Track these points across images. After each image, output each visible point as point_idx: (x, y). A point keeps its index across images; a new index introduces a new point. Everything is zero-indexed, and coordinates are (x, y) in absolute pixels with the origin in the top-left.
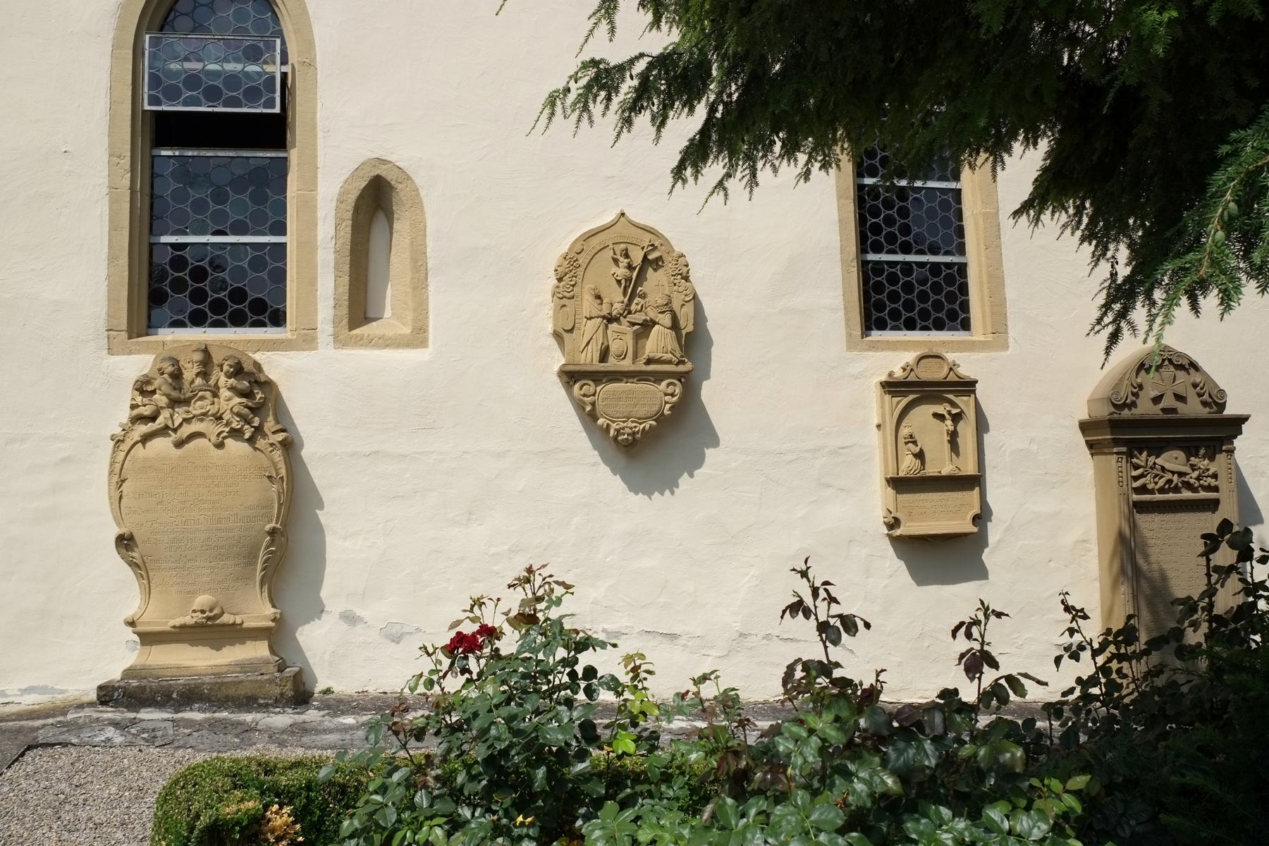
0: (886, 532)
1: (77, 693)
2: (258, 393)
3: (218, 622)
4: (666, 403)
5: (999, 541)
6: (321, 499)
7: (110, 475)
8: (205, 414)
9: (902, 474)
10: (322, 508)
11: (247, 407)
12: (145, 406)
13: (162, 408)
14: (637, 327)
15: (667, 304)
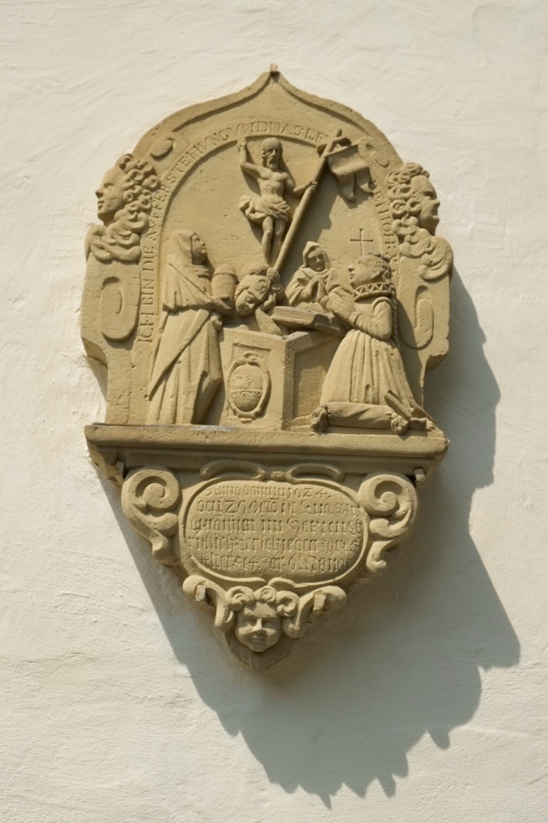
4: (374, 537)
14: (298, 334)
15: (378, 278)
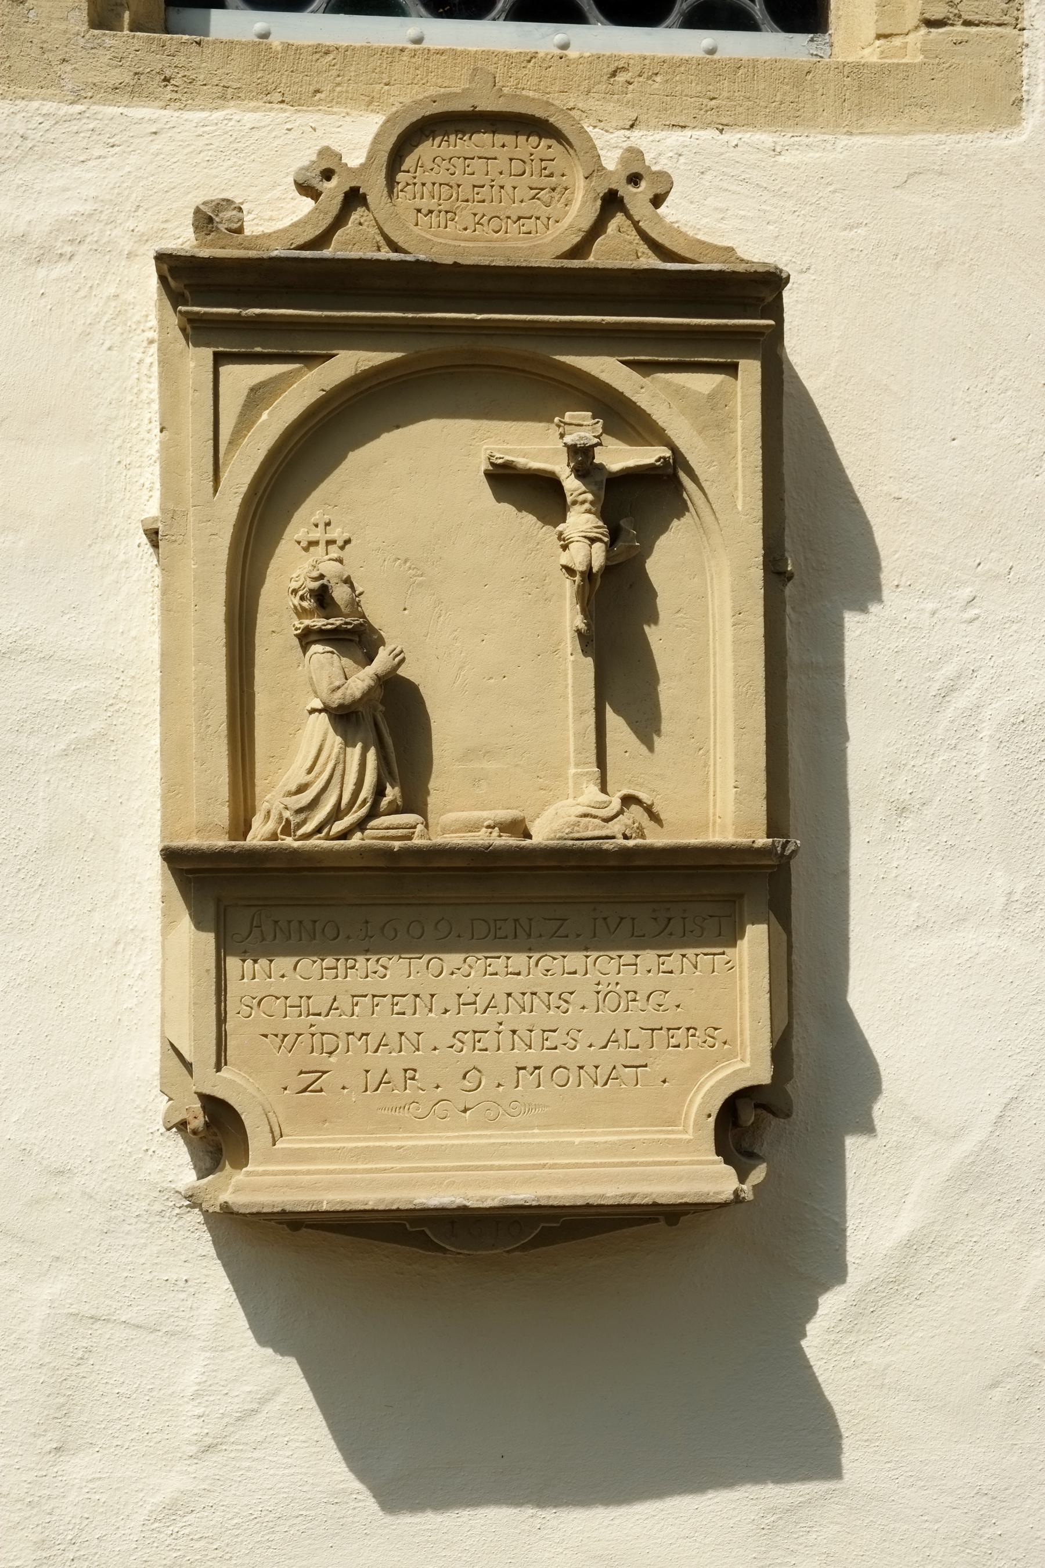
0: (187, 1177)
5: (911, 1246)
9: (258, 836)
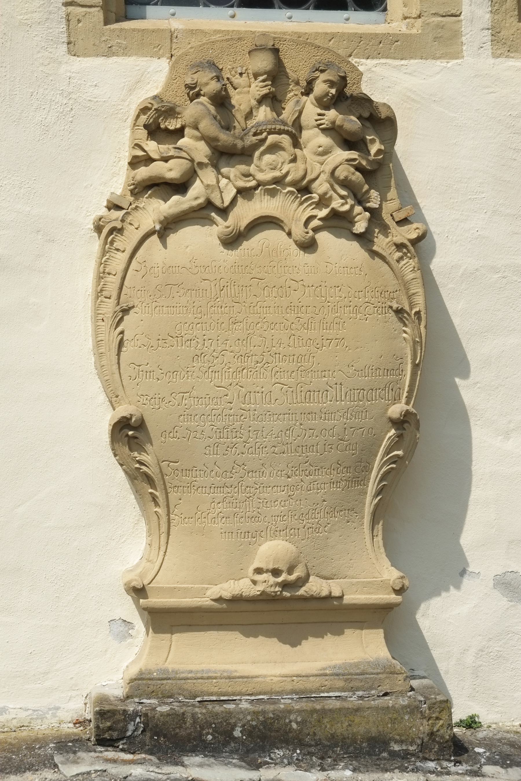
1: (23, 715)
2: (373, 141)
3: (302, 592)
6: (465, 357)
7: (97, 297)
8: (279, 181)
10: (465, 374)
11: (359, 168)
12: (166, 160)
13: (201, 165)
